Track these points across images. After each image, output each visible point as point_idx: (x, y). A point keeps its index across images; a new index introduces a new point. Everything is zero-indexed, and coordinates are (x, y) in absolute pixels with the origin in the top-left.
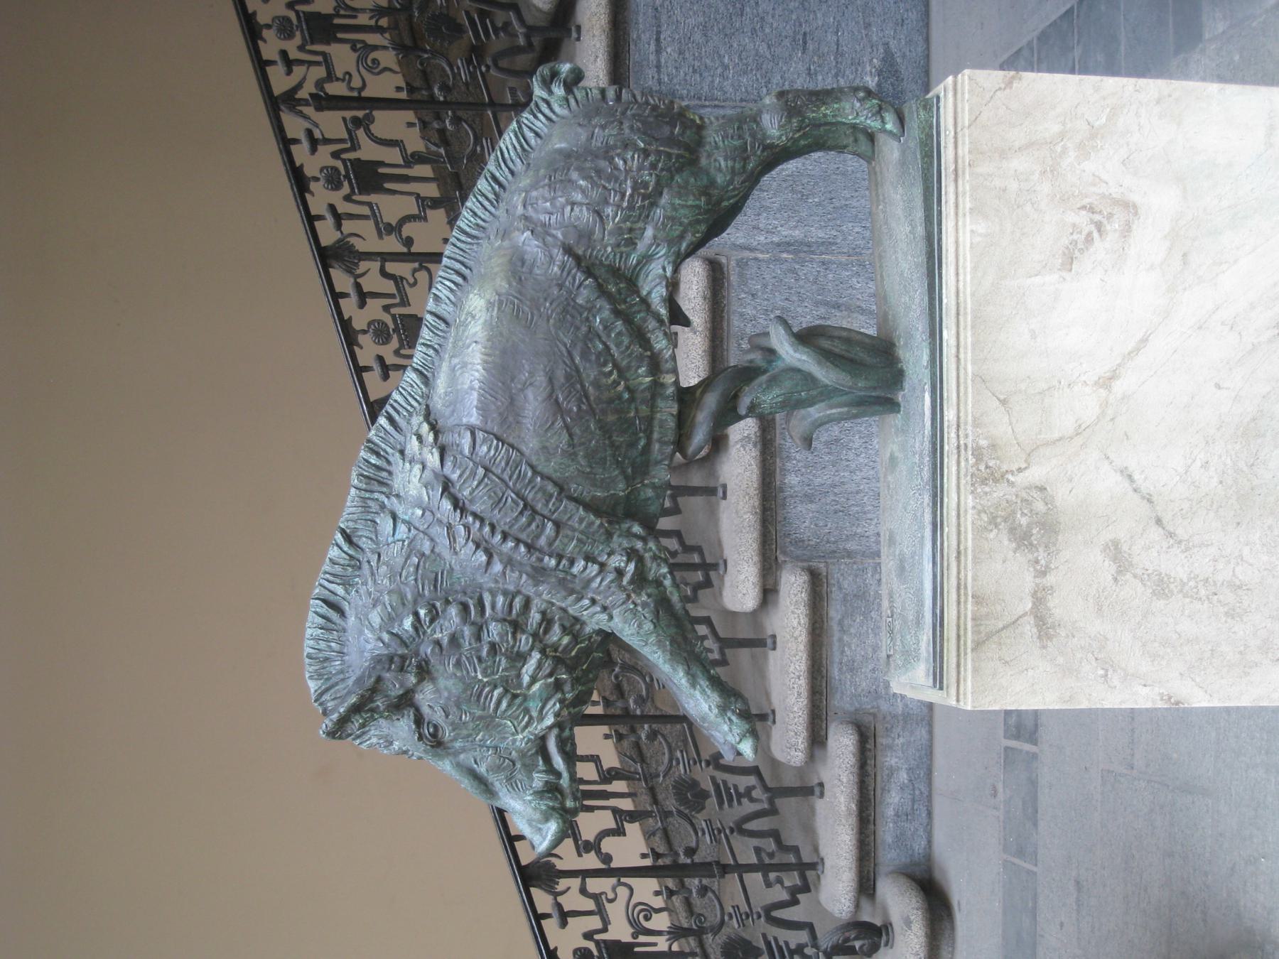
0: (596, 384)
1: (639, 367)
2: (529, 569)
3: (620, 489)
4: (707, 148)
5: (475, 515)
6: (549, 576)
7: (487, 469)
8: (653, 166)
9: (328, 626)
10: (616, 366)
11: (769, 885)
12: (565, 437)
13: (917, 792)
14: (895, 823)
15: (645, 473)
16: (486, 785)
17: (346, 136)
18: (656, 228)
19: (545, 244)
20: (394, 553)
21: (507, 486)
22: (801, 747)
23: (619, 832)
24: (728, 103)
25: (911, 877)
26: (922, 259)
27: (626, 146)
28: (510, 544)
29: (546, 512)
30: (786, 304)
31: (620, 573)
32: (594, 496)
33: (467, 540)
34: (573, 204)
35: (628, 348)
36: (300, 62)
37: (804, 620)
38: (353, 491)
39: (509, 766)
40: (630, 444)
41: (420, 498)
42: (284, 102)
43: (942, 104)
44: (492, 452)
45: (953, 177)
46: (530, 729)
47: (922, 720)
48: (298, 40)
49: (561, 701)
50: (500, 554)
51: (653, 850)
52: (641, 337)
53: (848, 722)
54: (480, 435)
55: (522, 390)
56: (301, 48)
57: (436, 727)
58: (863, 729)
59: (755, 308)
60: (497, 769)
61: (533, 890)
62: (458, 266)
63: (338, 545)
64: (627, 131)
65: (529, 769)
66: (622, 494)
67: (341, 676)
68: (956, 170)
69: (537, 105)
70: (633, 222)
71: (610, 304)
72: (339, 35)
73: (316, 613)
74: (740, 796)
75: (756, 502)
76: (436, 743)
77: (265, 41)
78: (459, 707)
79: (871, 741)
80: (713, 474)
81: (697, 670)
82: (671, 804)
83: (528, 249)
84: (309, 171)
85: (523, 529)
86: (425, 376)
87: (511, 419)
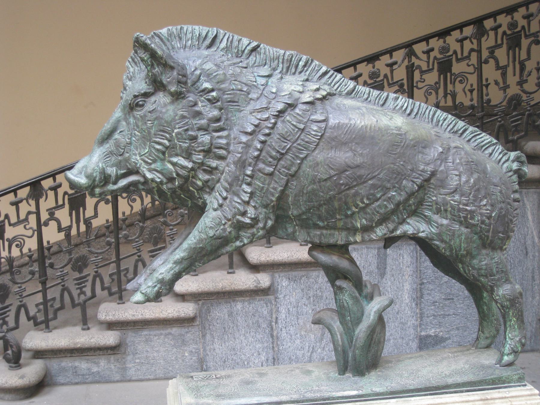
0: (356, 194)
1: (366, 219)
2: (244, 158)
3: (293, 212)
4: (491, 253)
5: (275, 124)
6: (240, 171)
7: (303, 130)
8: (483, 222)
9: (201, 39)
10: (367, 205)
11: (37, 305)
12: (325, 177)
13: (87, 377)
14: (71, 367)
15: (302, 227)
16: (107, 139)
18: (448, 225)
19: (436, 160)
20: (248, 76)
21: (293, 143)
22: (108, 318)
23: (60, 230)
25: (45, 376)
26: (434, 383)
27: (492, 205)
28: (259, 146)
29: (279, 167)
30: (324, 297)
31: (244, 214)
32: (289, 196)
33: (260, 120)
34: (459, 176)
35: (378, 212)
36: (429, 58)
37: (171, 316)
38: (282, 52)
39: (120, 151)
40: (326, 214)
41: (283, 91)
42: (410, 50)
43: (522, 388)
44: (314, 133)
45: (483, 398)
46: (143, 164)
47: (123, 377)
48: (439, 56)
49: (161, 183)
50: (252, 140)
51: (52, 247)
52: (384, 220)
53: (120, 340)
54: (323, 125)
55: (351, 150)
57: (142, 106)
58: (118, 348)
59: (322, 283)
60: (117, 145)
61: (28, 188)
62: (415, 111)
63: (250, 43)
64: (500, 206)
65: (118, 165)
66: (290, 213)
67: (170, 48)
68: (487, 399)
69: (506, 154)
70: (451, 212)
71: (403, 200)
72: (442, 76)
73: (209, 31)
74: (81, 289)
75: (228, 289)
76: (133, 106)
78: (156, 119)
79: (112, 352)
80: (238, 267)
81: (185, 264)
82: (74, 256)
83: (432, 150)
84: (377, 63)
85: (268, 153)
86: (352, 93)
87: (334, 143)
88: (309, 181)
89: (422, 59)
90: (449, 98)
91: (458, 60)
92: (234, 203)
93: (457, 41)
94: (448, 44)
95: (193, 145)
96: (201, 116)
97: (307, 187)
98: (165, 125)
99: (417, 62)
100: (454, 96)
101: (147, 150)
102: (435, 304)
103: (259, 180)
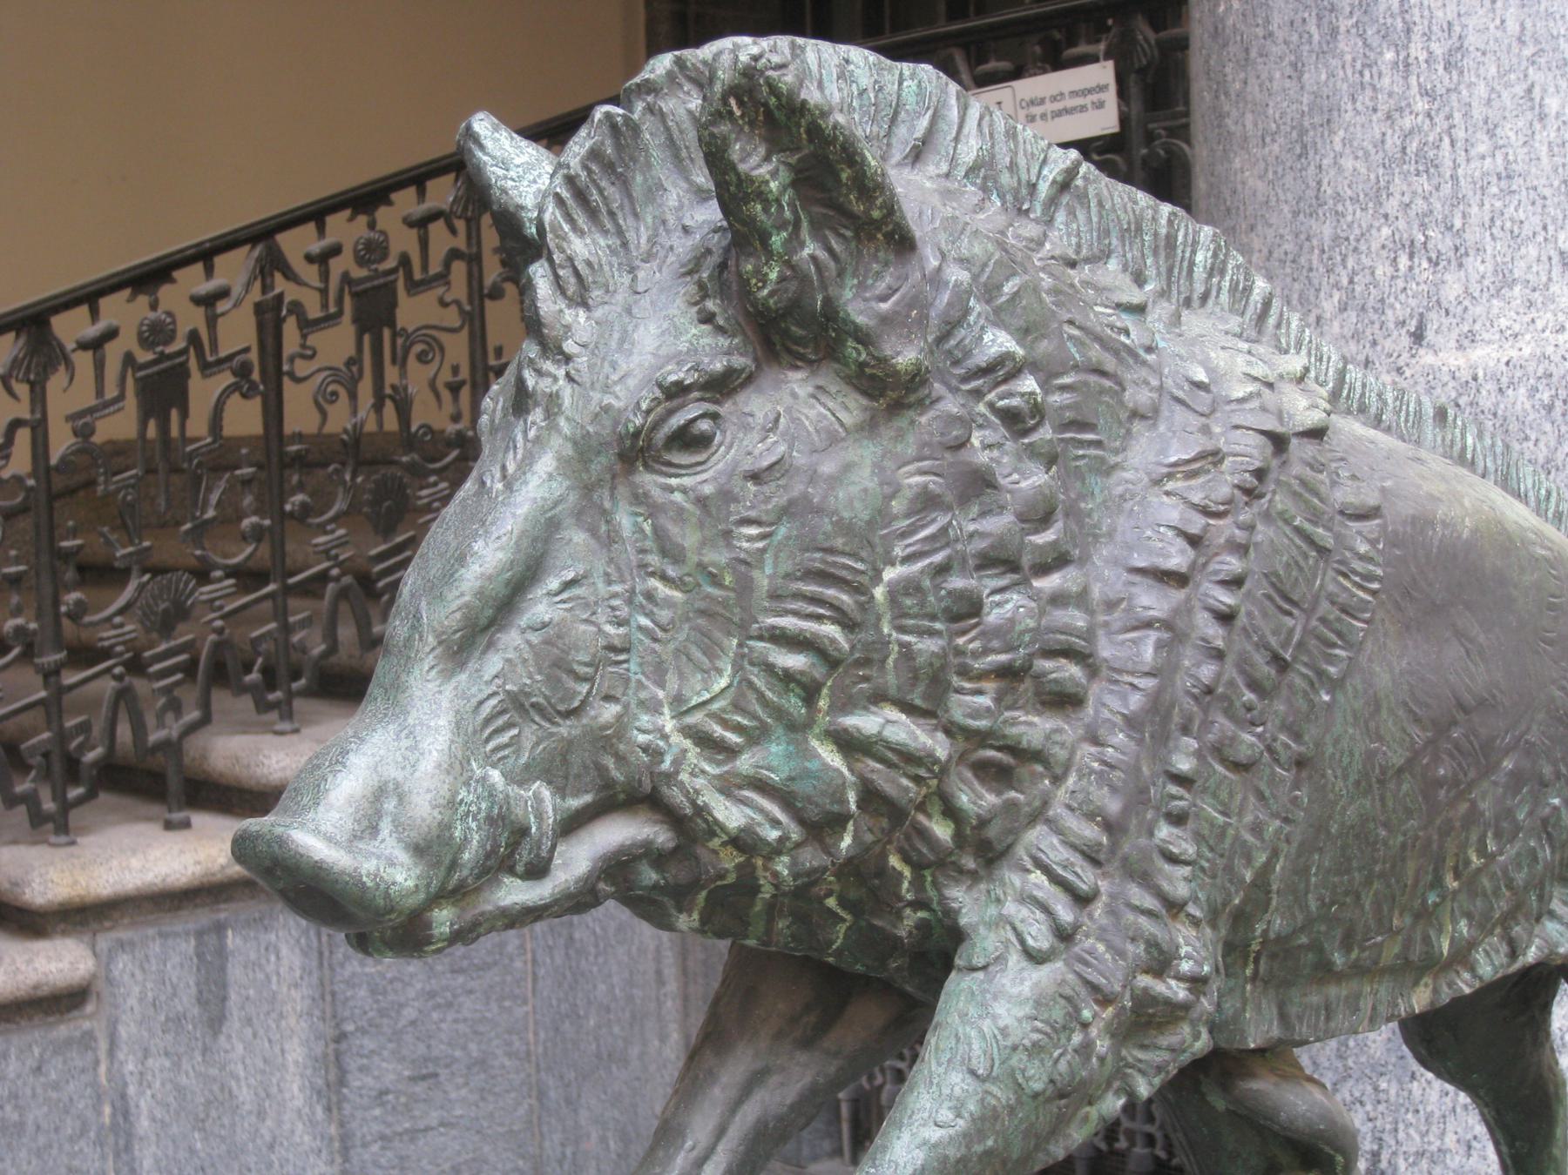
17: (223, 354)
24: (327, 972)
30: (30, 1128)
36: (325, 276)
46: (693, 753)
48: (359, 273)
56: (346, 278)
57: (703, 442)
59: (19, 1076)
65: (553, 769)
72: (367, 338)
77: (351, 219)
78: (786, 511)
84: (166, 292)
88: (1351, 780)
89: (306, 279)
90: (389, 409)
91: (414, 287)
92: (1131, 917)
93: (410, 223)
94: (383, 233)
95: (961, 641)
96: (989, 496)
97: (1344, 809)
98: (839, 542)
99: (291, 292)
100: (404, 408)
101: (723, 682)
102: (385, 1098)
103: (1215, 796)
